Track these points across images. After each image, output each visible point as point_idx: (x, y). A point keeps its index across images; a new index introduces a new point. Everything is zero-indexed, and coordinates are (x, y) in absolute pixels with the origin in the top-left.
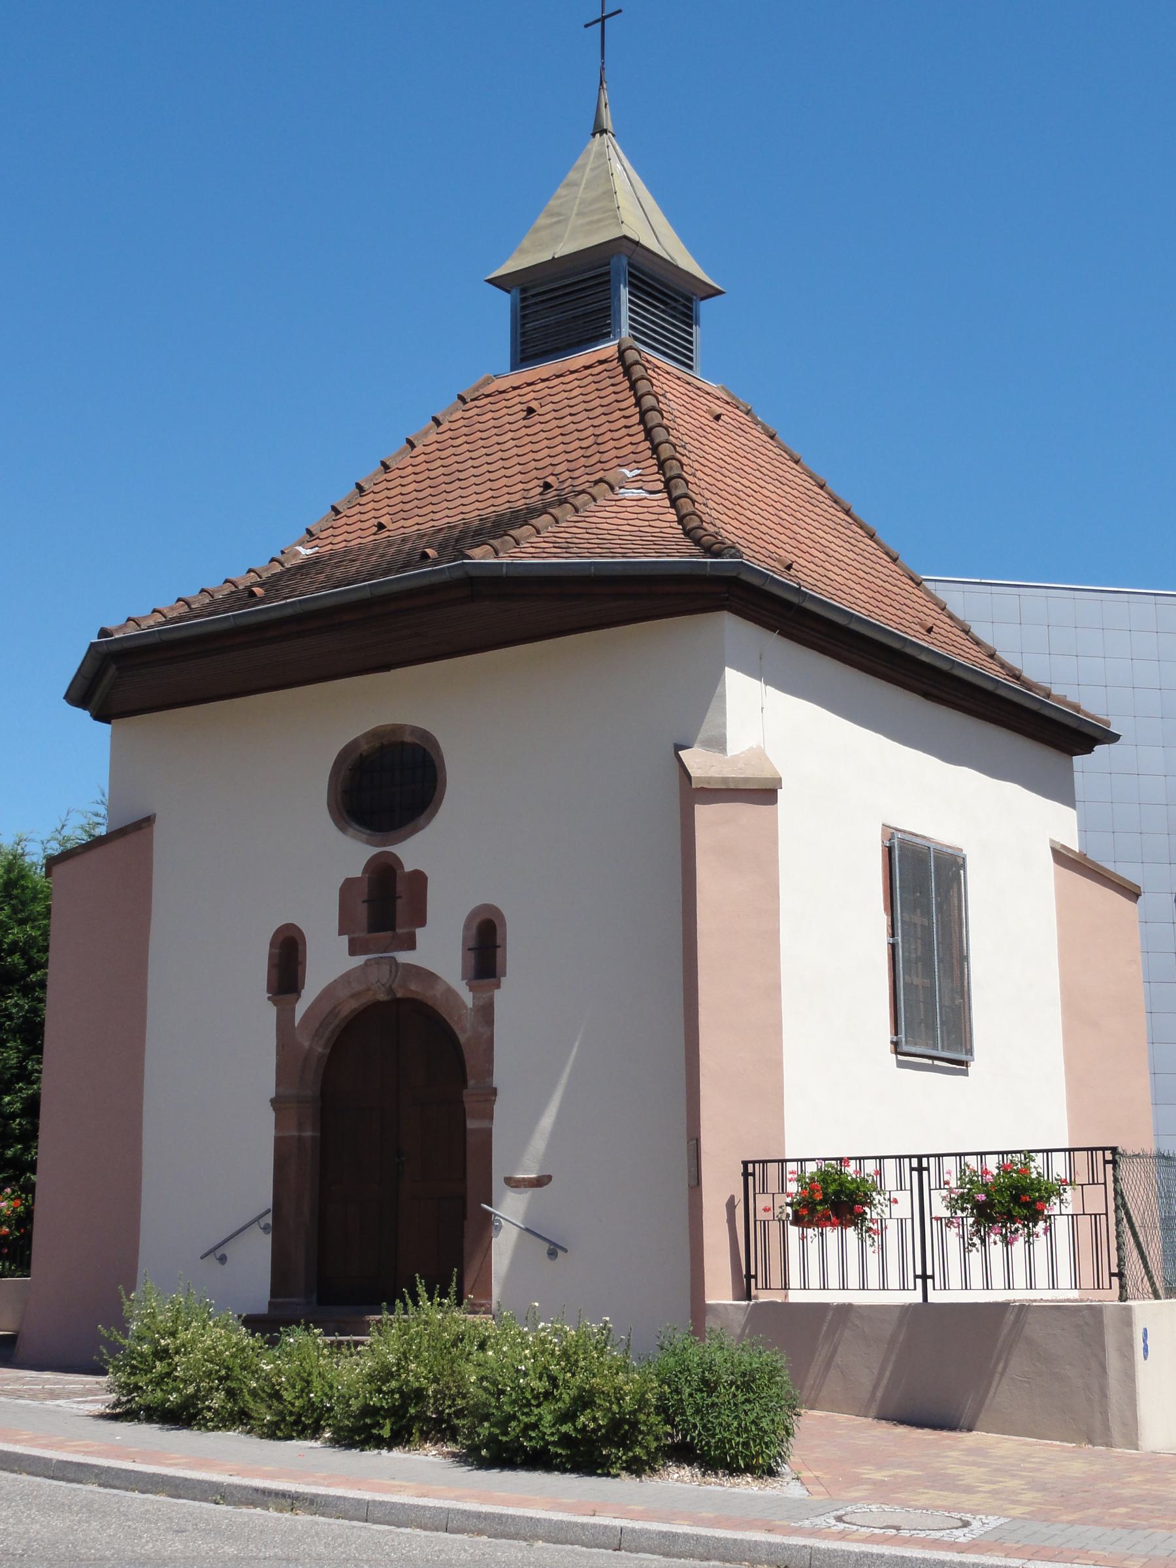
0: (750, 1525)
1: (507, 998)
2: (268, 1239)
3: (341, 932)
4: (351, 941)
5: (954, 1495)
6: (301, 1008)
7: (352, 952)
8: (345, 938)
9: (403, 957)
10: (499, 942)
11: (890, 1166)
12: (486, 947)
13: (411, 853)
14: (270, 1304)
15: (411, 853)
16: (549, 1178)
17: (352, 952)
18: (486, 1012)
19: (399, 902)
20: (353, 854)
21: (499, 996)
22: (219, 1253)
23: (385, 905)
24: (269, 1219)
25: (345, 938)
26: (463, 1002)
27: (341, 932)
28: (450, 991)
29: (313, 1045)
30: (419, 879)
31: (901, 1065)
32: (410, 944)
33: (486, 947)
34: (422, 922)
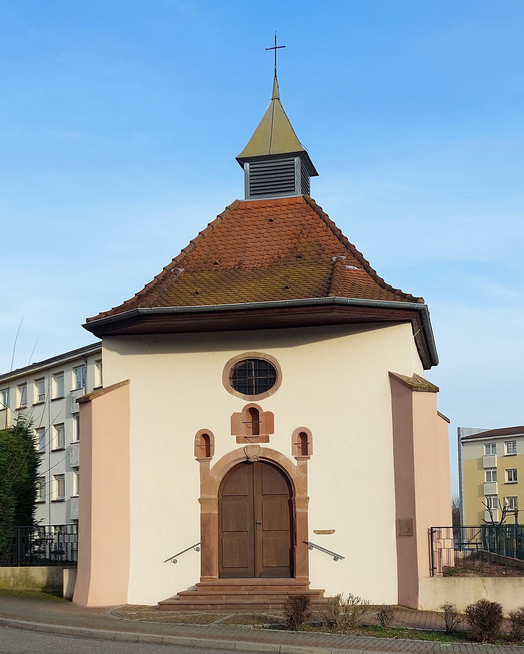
0: (33, 620)
2: (198, 555)
5: (82, 640)
6: (212, 463)
7: (238, 442)
8: (235, 436)
9: (262, 445)
12: (303, 439)
13: (266, 404)
17: (238, 442)
18: (304, 469)
20: (239, 403)
21: (310, 463)
23: (256, 422)
24: (199, 546)
25: (235, 436)
26: (293, 464)
28: (286, 459)
29: (218, 478)
30: (270, 416)
31: (428, 529)
32: (267, 440)
33: (303, 439)
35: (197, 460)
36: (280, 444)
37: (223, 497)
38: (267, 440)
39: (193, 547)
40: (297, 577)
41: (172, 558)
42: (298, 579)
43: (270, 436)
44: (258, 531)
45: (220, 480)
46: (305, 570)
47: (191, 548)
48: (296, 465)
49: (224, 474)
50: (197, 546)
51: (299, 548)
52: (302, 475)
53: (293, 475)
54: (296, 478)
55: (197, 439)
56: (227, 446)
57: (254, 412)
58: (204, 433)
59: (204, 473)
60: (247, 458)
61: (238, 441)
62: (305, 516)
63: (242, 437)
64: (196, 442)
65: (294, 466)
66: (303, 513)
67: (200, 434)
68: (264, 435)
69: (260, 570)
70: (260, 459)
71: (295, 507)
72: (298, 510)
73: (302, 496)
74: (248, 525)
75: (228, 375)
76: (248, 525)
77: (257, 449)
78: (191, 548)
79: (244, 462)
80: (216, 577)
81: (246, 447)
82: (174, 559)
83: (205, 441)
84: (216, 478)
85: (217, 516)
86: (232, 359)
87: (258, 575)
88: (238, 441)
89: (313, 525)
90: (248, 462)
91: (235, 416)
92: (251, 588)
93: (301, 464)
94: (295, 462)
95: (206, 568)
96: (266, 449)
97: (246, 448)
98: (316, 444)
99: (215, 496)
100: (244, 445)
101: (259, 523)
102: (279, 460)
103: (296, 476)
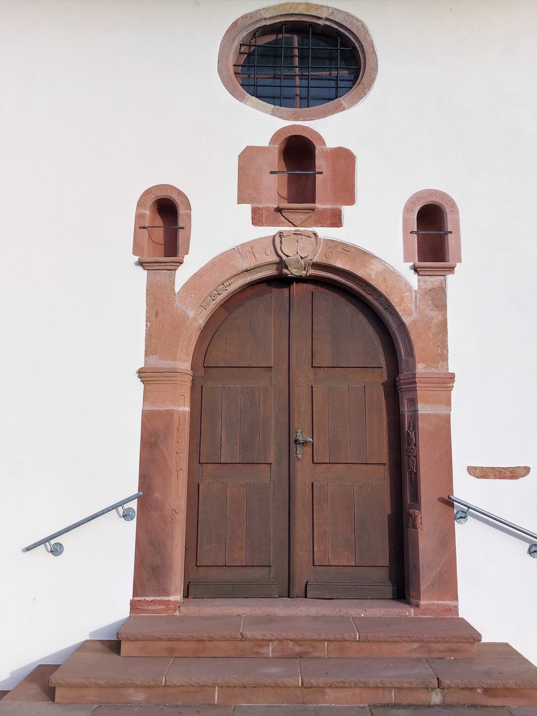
1: (458, 285)
3: (241, 200)
4: (255, 211)
6: (182, 276)
8: (247, 208)
9: (325, 232)
10: (450, 227)
11: (262, 11)
12: (432, 227)
13: (331, 129)
14: (133, 605)
15: (331, 129)
16: (526, 470)
18: (438, 298)
19: (318, 177)
20: (262, 125)
22: (292, 441)
24: (134, 505)
25: (247, 208)
26: (406, 283)
27: (241, 200)
28: (389, 272)
29: (196, 317)
30: (345, 159)
32: (336, 220)
33: (432, 227)
34: (351, 200)
35: (141, 264)
36: (372, 232)
37: (206, 367)
38: (336, 220)
39: (115, 507)
40: (423, 602)
41: (48, 539)
42: (427, 609)
43: (346, 210)
44: (298, 465)
45: (201, 322)
46: (448, 584)
47: (108, 510)
48: (415, 287)
49: (212, 306)
50: (126, 506)
51: (426, 518)
52: (434, 313)
53: (410, 310)
54: (414, 322)
55: (142, 211)
56: (224, 231)
57: (298, 152)
58: (162, 194)
59: (158, 303)
60: (281, 264)
61: (258, 218)
62: (444, 426)
63: (267, 209)
64: (139, 217)
65: (410, 289)
66: (438, 417)
67: (152, 199)
68: (329, 206)
69: (303, 572)
70: (312, 272)
71: (413, 402)
72: (423, 409)
73: (434, 370)
74: (273, 447)
75: (232, 59)
76: (273, 447)
77: (306, 244)
78: (108, 510)
79: (268, 281)
80: (177, 597)
81: (281, 234)
82: (53, 542)
83: (166, 217)
84: (191, 314)
85: (188, 418)
86: (246, 16)
87: (298, 588)
88: (258, 218)
89: (465, 452)
90: (281, 281)
91: (248, 157)
92: (297, 649)
93: (429, 286)
94: (413, 279)
95: (148, 572)
96: (332, 244)
97: (143, 379)
98: (469, 233)
99: (185, 365)
100: (271, 231)
101: (305, 443)
102: (370, 273)
103: (415, 315)
